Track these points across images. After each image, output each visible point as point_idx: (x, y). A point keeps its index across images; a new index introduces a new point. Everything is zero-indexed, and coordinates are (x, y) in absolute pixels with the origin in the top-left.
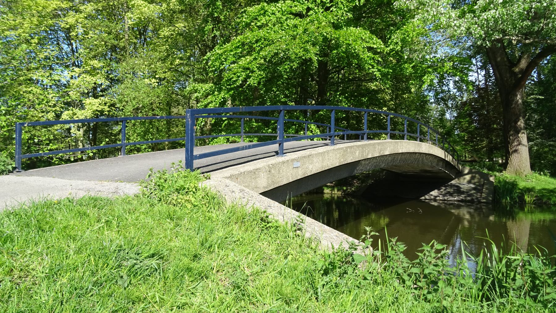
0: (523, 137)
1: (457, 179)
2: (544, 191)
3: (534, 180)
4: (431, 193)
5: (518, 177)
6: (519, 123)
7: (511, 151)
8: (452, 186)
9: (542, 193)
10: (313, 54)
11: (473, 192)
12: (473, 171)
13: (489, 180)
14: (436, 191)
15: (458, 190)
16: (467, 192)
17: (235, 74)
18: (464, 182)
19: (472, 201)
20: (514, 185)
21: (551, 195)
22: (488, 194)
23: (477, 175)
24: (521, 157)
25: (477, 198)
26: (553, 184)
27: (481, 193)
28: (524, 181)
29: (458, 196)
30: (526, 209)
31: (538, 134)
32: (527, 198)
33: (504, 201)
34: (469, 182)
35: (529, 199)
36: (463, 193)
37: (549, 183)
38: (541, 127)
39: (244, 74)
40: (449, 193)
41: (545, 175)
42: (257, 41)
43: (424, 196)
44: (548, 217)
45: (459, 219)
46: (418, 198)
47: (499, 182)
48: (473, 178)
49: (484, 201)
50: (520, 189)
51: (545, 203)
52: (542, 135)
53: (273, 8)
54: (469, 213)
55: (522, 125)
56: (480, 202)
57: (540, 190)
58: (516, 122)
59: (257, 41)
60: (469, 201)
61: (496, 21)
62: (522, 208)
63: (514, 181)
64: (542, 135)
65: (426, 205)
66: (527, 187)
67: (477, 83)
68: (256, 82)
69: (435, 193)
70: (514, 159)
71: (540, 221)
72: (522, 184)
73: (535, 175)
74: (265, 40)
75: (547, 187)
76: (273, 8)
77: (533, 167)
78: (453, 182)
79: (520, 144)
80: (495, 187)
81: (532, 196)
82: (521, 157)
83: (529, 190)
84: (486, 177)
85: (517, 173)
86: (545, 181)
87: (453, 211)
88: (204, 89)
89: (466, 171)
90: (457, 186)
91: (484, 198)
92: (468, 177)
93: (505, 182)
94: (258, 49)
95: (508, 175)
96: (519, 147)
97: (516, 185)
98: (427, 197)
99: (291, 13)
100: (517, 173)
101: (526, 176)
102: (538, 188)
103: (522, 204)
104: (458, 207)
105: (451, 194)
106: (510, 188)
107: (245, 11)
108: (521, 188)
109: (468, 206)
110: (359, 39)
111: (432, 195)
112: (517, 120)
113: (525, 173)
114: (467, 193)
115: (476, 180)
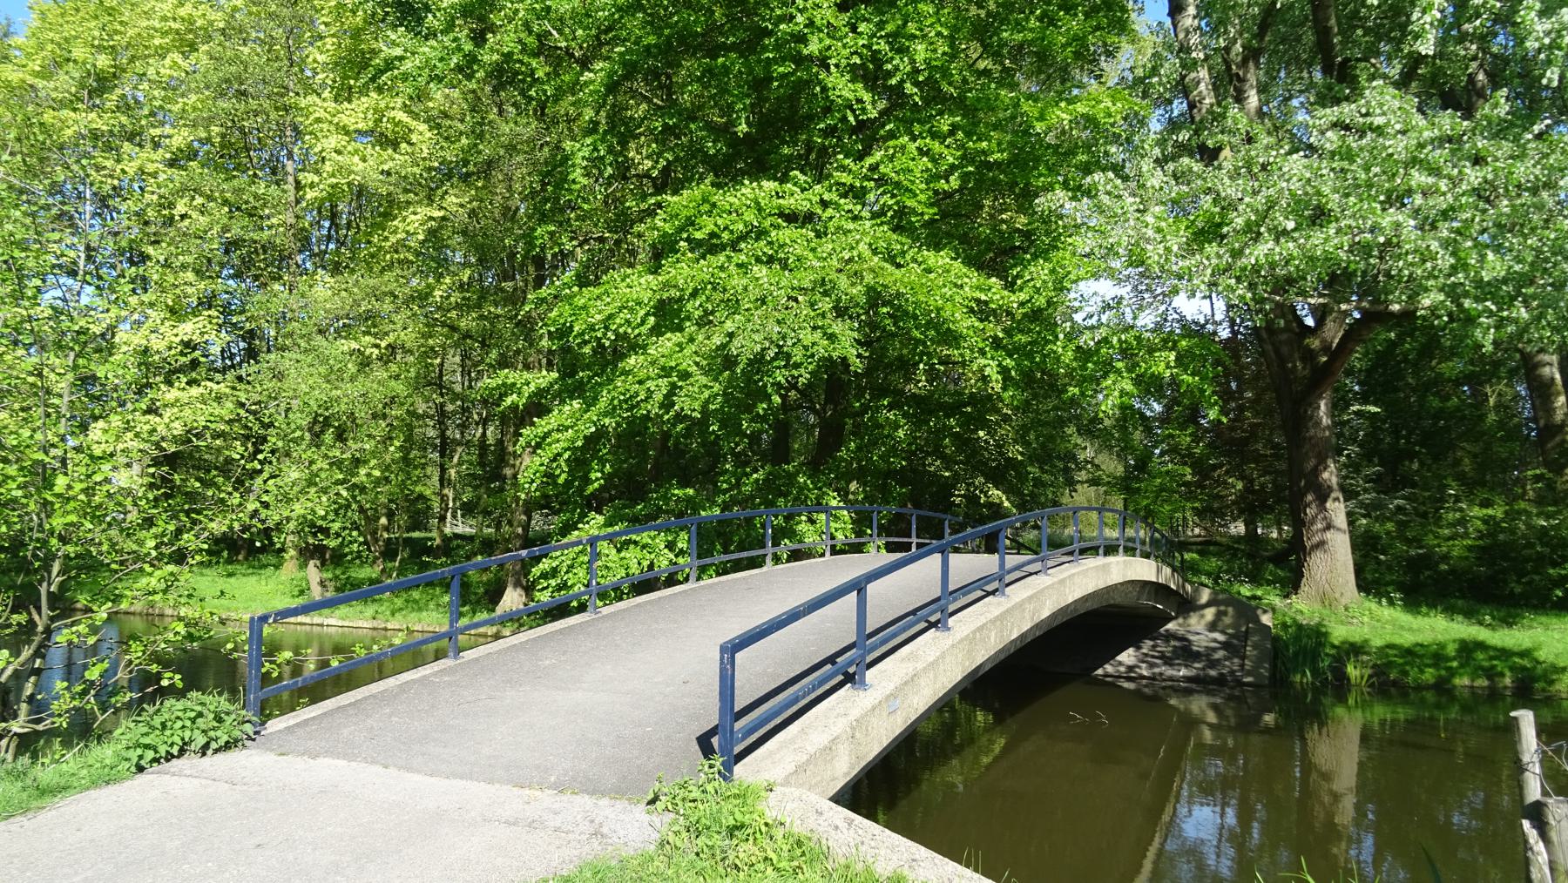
0: (1338, 510)
1: (1180, 620)
2: (1391, 652)
3: (1366, 619)
4: (1119, 658)
5: (1326, 612)
6: (1326, 475)
7: (1308, 545)
8: (1170, 636)
9: (1387, 655)
10: (846, 344)
11: (1220, 654)
12: (1221, 597)
13: (1257, 621)
14: (1131, 651)
15: (1185, 652)
16: (1208, 655)
17: (640, 382)
18: (1199, 628)
19: (1221, 681)
20: (1317, 635)
21: (1406, 663)
22: (1258, 662)
23: (1230, 610)
24: (1334, 558)
25: (1232, 672)
26: (1410, 629)
27: (1243, 658)
28: (1342, 623)
29: (1186, 666)
30: (1351, 701)
31: (1368, 480)
32: (1352, 671)
33: (1298, 678)
34: (1212, 627)
35: (1358, 673)
36: (1197, 656)
37: (1402, 627)
38: (1376, 460)
39: (663, 382)
40: (1162, 657)
41: (1391, 603)
42: (694, 294)
43: (1101, 666)
44: (1403, 713)
45: (1191, 723)
46: (1085, 674)
47: (1285, 626)
48: (1219, 615)
49: (1250, 679)
50: (1334, 646)
51: (1394, 683)
52: (1377, 480)
53: (732, 200)
54: (1215, 707)
55: (1334, 480)
56: (1240, 684)
57: (1381, 649)
58: (1316, 472)
59: (694, 294)
60: (1214, 681)
61: (1273, 265)
62: (1341, 698)
63: (1320, 624)
64: (1377, 480)
65: (1109, 685)
66: (1352, 640)
67: (1210, 327)
68: (697, 405)
69: (1127, 657)
70: (1317, 566)
71: (1383, 722)
72: (1339, 633)
73: (1367, 604)
74: (714, 289)
75: (1398, 640)
76: (732, 200)
77: (1364, 585)
78: (1171, 626)
79: (1329, 527)
80: (1276, 639)
81: (1364, 665)
82: (1334, 558)
83: (1354, 650)
84: (1247, 611)
85: (1325, 599)
86: (1393, 622)
87: (1173, 702)
88: (532, 387)
89: (1205, 595)
90: (1183, 639)
91: (1249, 674)
92: (1210, 613)
93: (1300, 627)
94: (698, 313)
95: (1303, 607)
96: (1329, 535)
97: (1326, 634)
98: (1109, 668)
99: (781, 215)
100: (1325, 599)
101: (1346, 609)
102: (1377, 642)
103: (1340, 686)
104: (1188, 692)
105: (1168, 661)
106: (1310, 640)
107: (659, 205)
108: (1336, 643)
109: (1209, 693)
110: (944, 283)
111: (1120, 663)
112: (1322, 463)
113: (1344, 601)
114: (1206, 656)
115: (1227, 620)
